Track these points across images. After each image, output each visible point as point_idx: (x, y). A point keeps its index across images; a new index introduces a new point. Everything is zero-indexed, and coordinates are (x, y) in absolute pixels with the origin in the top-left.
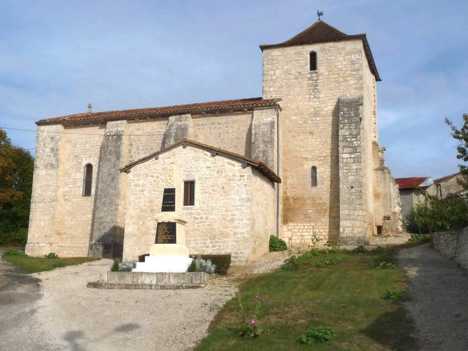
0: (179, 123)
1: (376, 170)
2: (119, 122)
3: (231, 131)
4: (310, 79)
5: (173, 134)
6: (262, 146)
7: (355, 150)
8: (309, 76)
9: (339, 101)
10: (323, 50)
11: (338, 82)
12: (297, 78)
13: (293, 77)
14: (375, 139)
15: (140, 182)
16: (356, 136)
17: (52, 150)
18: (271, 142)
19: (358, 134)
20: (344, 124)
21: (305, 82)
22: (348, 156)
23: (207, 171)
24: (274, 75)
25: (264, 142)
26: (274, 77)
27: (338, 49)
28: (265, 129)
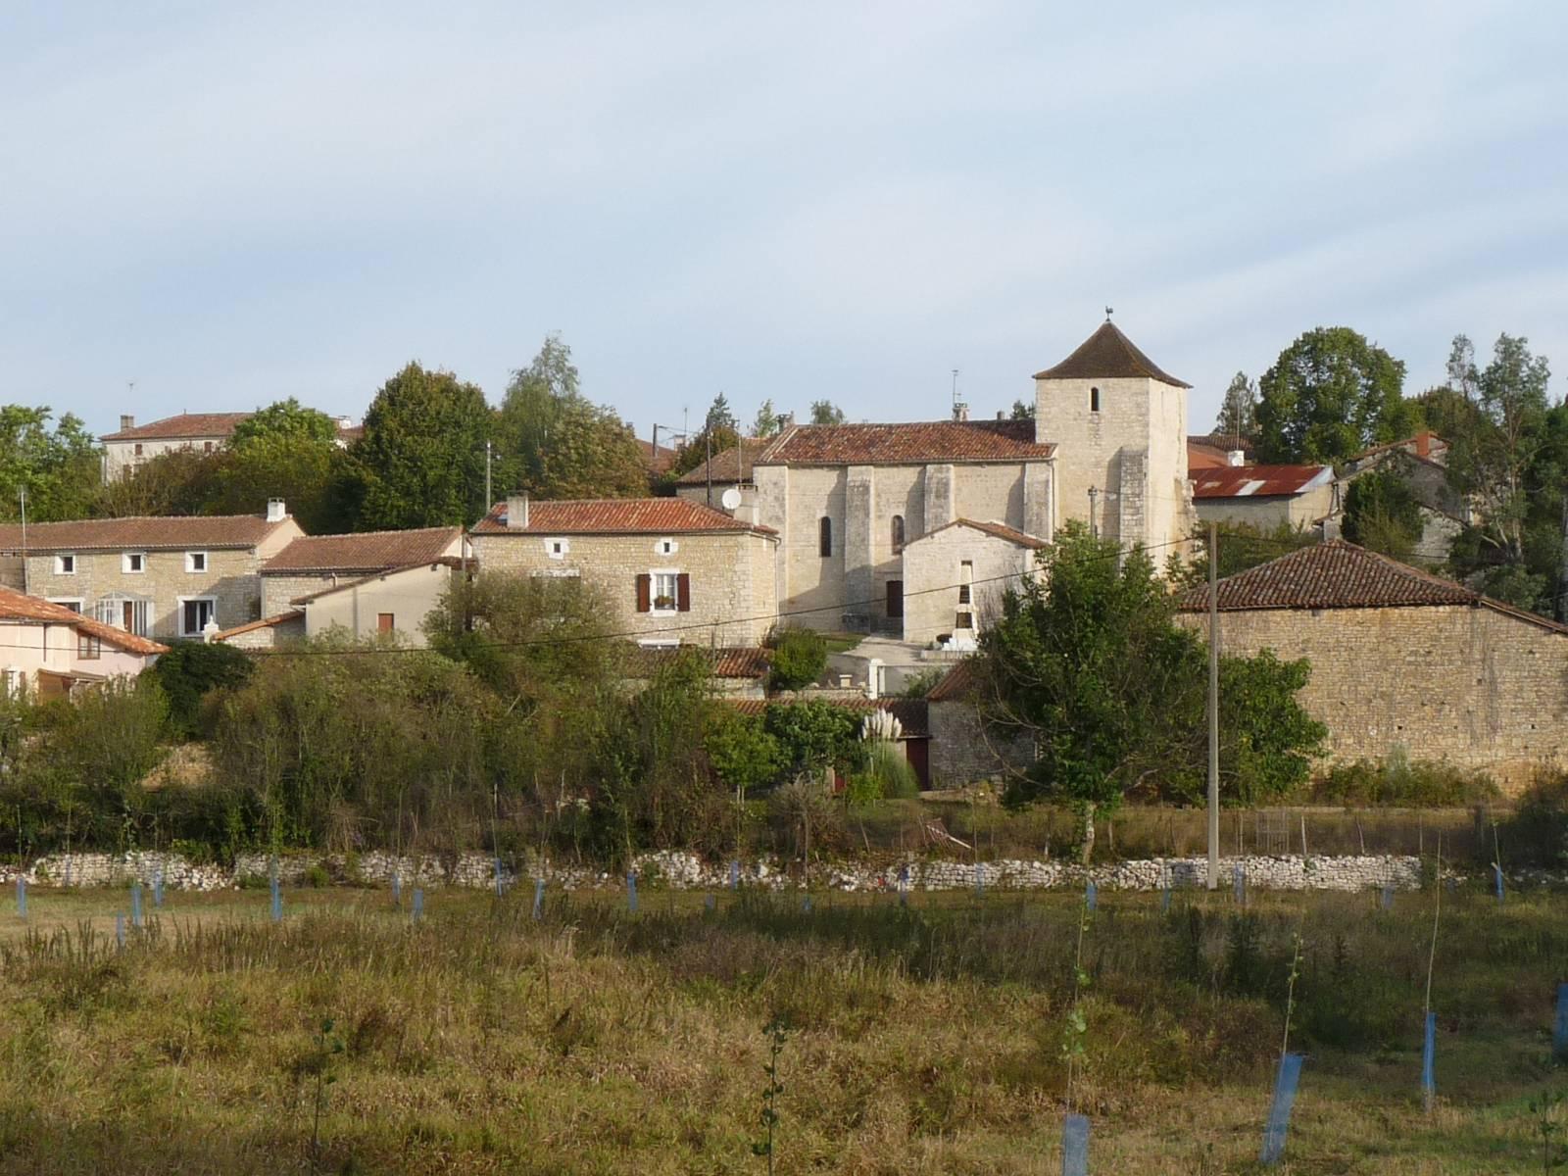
0: (939, 475)
1: (1179, 513)
2: (864, 468)
3: (1000, 485)
4: (1091, 422)
5: (934, 490)
6: (1035, 508)
7: (1137, 511)
8: (1090, 417)
9: (1121, 452)
10: (1106, 387)
11: (1122, 427)
12: (1075, 419)
13: (1072, 417)
14: (1177, 475)
15: (917, 561)
16: (1138, 496)
17: (776, 498)
18: (1046, 504)
19: (1141, 493)
20: (1127, 482)
21: (1086, 426)
22: (1130, 517)
23: (983, 552)
24: (1050, 413)
25: (1038, 503)
26: (1050, 416)
27: (1123, 388)
28: (1039, 488)
